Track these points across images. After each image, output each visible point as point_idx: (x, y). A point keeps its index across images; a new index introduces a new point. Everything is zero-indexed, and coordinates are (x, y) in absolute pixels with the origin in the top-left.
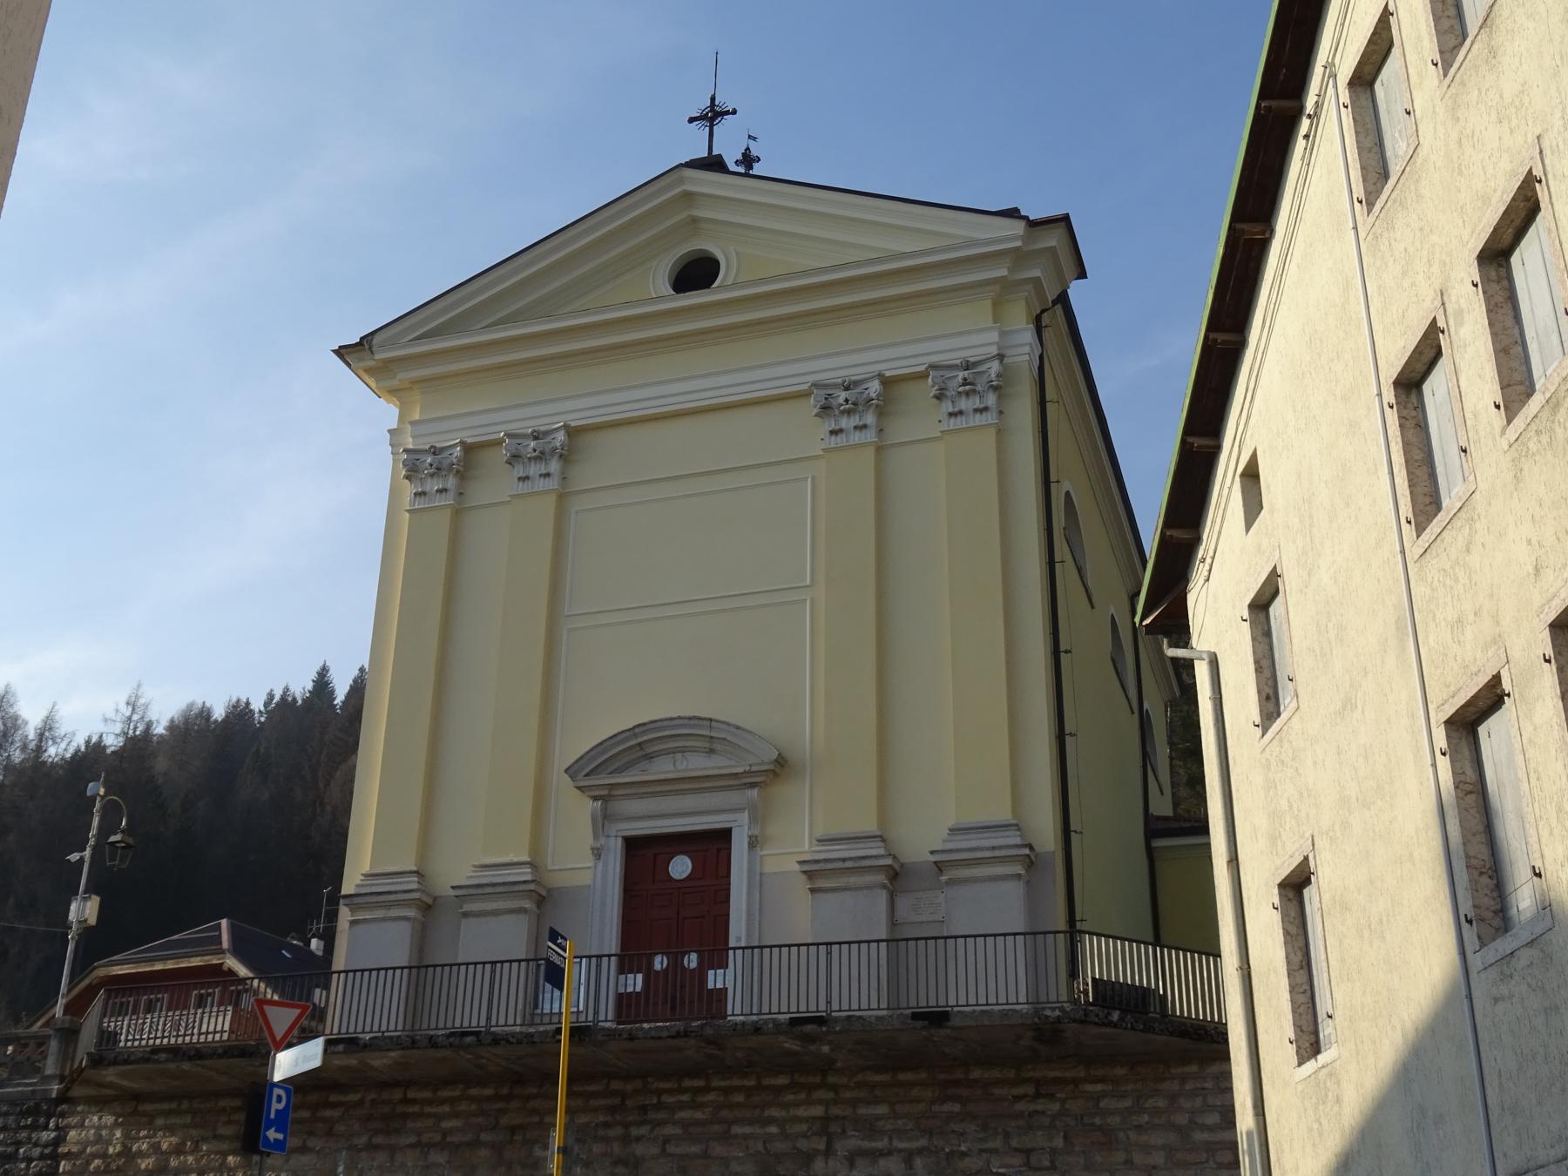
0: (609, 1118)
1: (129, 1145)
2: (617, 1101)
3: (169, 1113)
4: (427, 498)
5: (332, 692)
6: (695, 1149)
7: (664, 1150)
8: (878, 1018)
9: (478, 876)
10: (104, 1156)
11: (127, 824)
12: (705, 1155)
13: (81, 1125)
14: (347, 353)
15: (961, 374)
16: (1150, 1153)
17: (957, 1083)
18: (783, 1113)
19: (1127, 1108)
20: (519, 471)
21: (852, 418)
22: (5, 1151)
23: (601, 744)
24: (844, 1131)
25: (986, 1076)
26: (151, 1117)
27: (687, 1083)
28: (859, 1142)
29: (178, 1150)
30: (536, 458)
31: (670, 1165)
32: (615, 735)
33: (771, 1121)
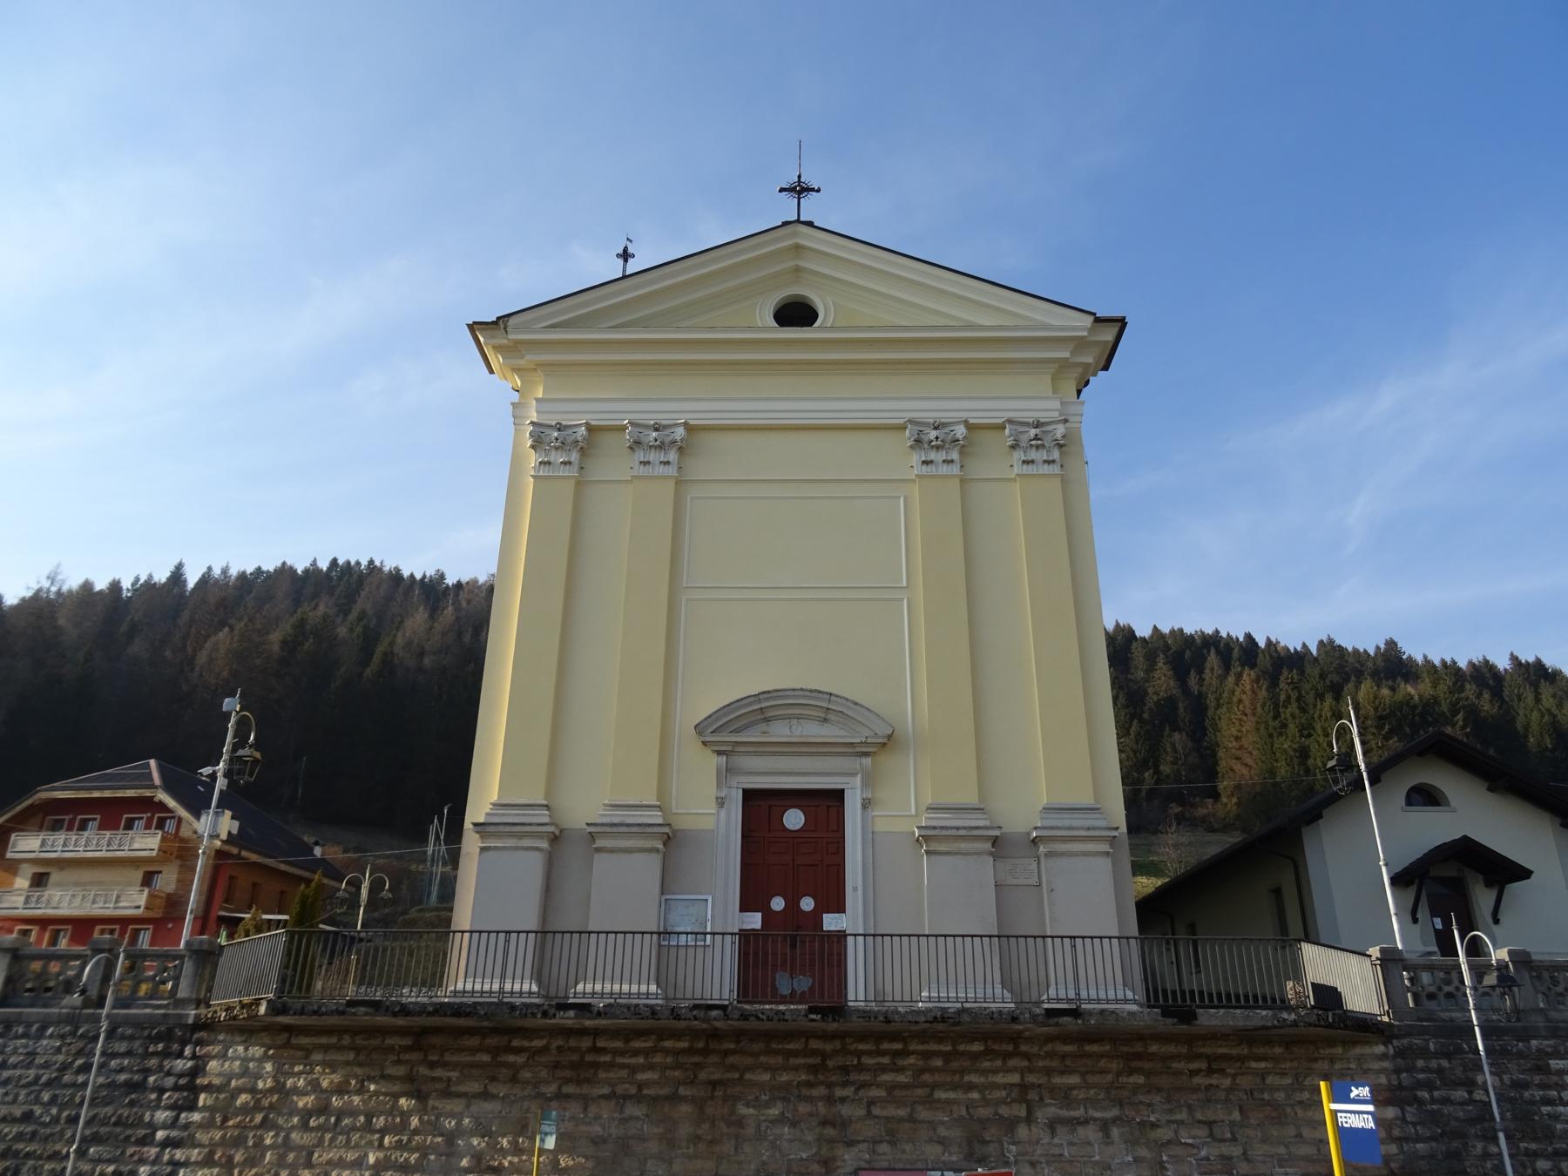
0: (812, 1078)
1: (282, 1080)
2: (817, 1060)
3: (326, 1048)
4: (551, 467)
5: (185, 581)
6: (902, 1112)
7: (869, 1112)
8: (1131, 1014)
10: (253, 1090)
11: (255, 739)
12: (911, 1119)
13: (223, 1056)
14: (479, 329)
15: (1033, 432)
16: (1315, 1128)
17: (1138, 1056)
18: (983, 1080)
20: (640, 455)
22: (132, 1079)
24: (1041, 1099)
25: (1163, 1050)
27: (885, 1046)
29: (341, 1090)
30: (656, 447)
31: (877, 1127)
33: (970, 1087)
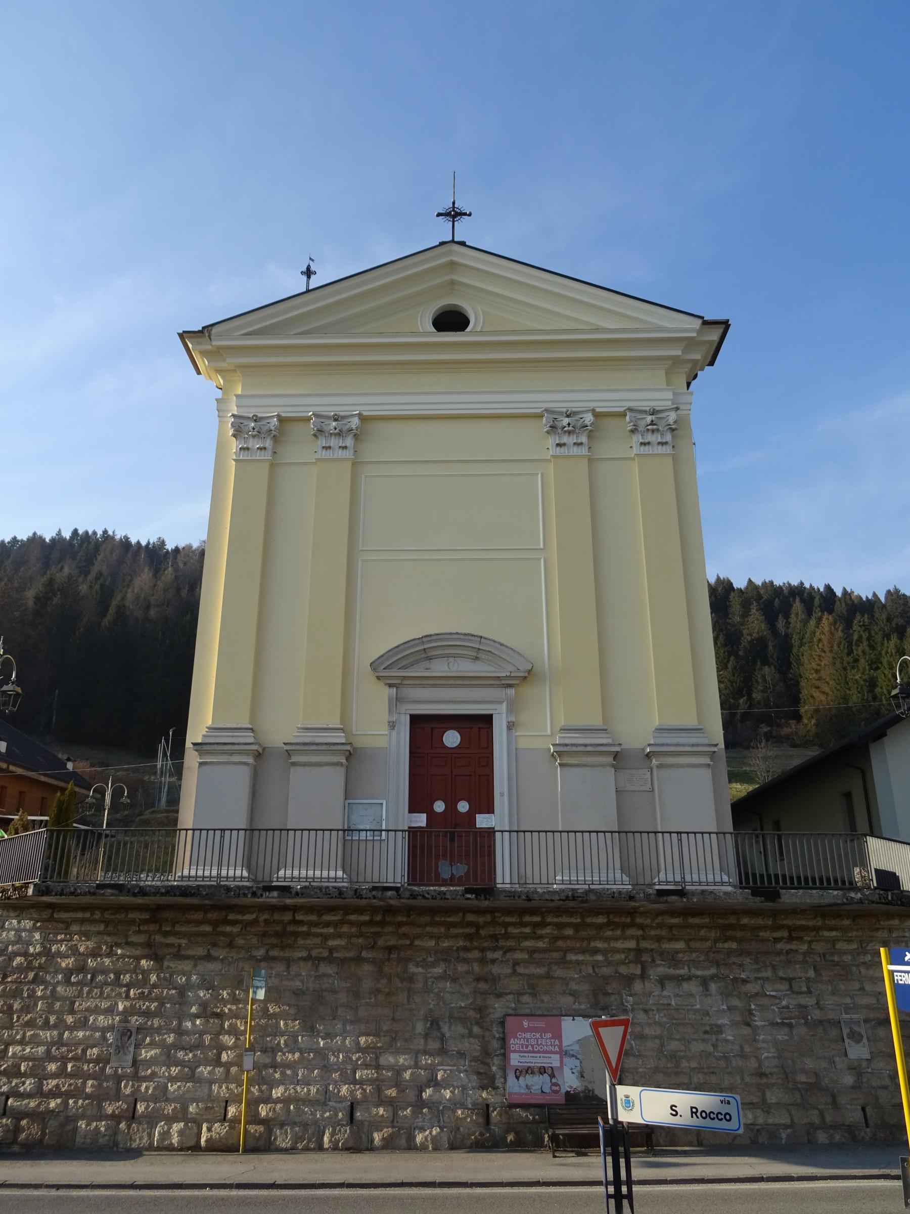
0: (468, 944)
3: (82, 921)
6: (541, 971)
7: (514, 971)
9: (302, 736)
10: (25, 954)
11: (16, 677)
15: (649, 418)
16: (876, 983)
17: (732, 927)
18: (606, 945)
19: (854, 949)
20: (322, 442)
21: (571, 436)
23: (397, 647)
24: (653, 961)
25: (753, 922)
26: (67, 924)
27: (527, 919)
28: (667, 969)
29: (95, 953)
30: (335, 434)
31: (521, 982)
32: (409, 641)
33: (596, 951)
